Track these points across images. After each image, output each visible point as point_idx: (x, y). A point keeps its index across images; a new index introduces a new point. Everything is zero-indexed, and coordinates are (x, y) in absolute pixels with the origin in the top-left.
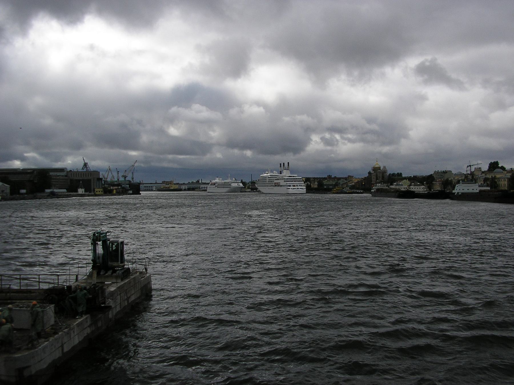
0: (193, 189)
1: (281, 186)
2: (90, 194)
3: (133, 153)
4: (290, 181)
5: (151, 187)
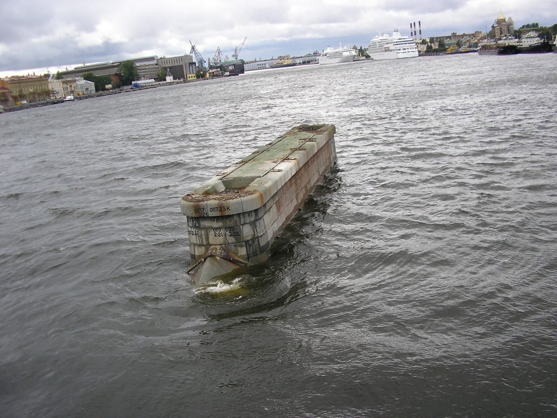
0: (309, 62)
1: (391, 50)
2: (179, 81)
4: (400, 44)
5: (265, 64)
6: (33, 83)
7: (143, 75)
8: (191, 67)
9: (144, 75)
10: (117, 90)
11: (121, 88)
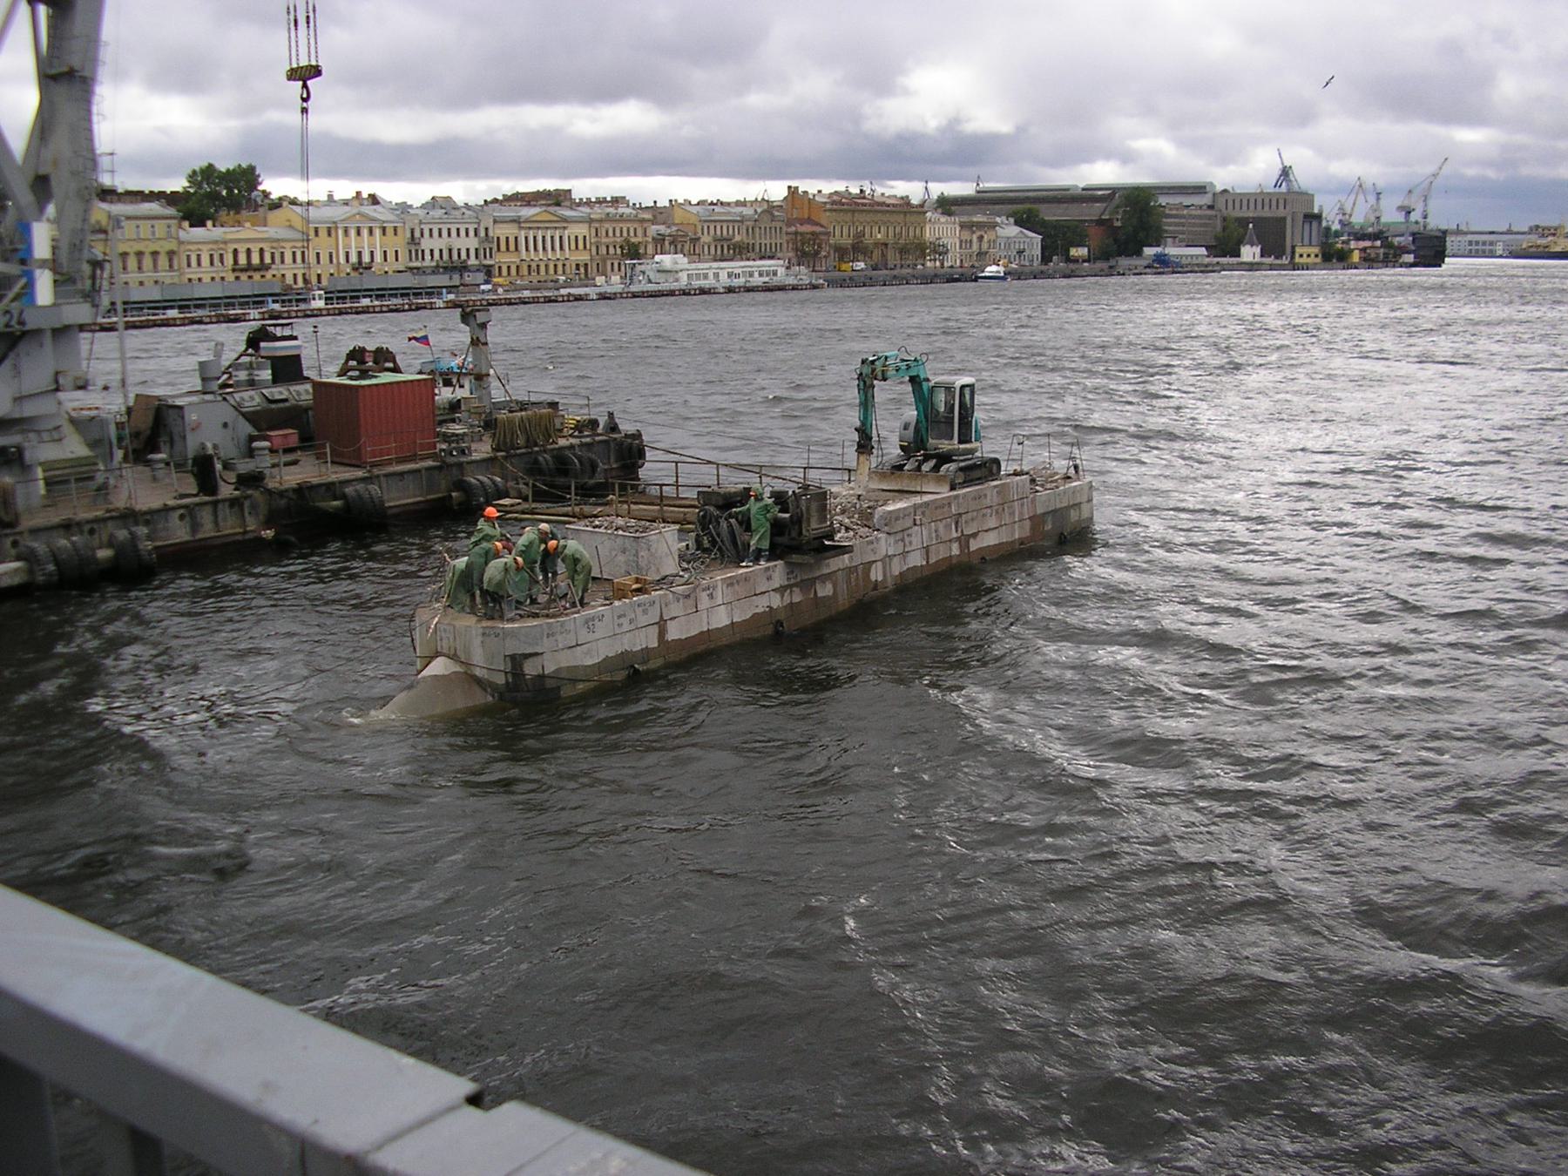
3: (1469, 136)
5: (1491, 243)
7: (1171, 232)
8: (1307, 227)
9: (1175, 232)
10: (1099, 265)
11: (1112, 262)
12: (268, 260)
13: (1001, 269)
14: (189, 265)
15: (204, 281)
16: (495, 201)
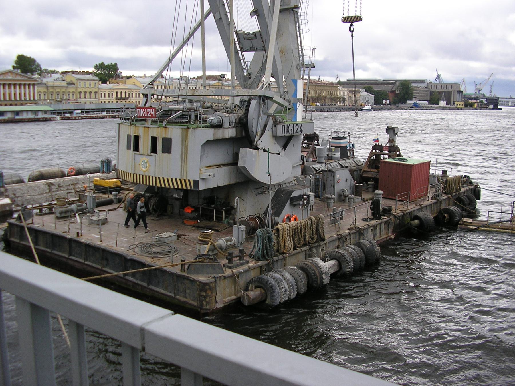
5: (507, 102)
6: (326, 88)
8: (458, 95)
10: (393, 106)
11: (397, 105)
12: (127, 96)
13: (370, 107)
14: (101, 97)
15: (106, 102)
16: (194, 78)
